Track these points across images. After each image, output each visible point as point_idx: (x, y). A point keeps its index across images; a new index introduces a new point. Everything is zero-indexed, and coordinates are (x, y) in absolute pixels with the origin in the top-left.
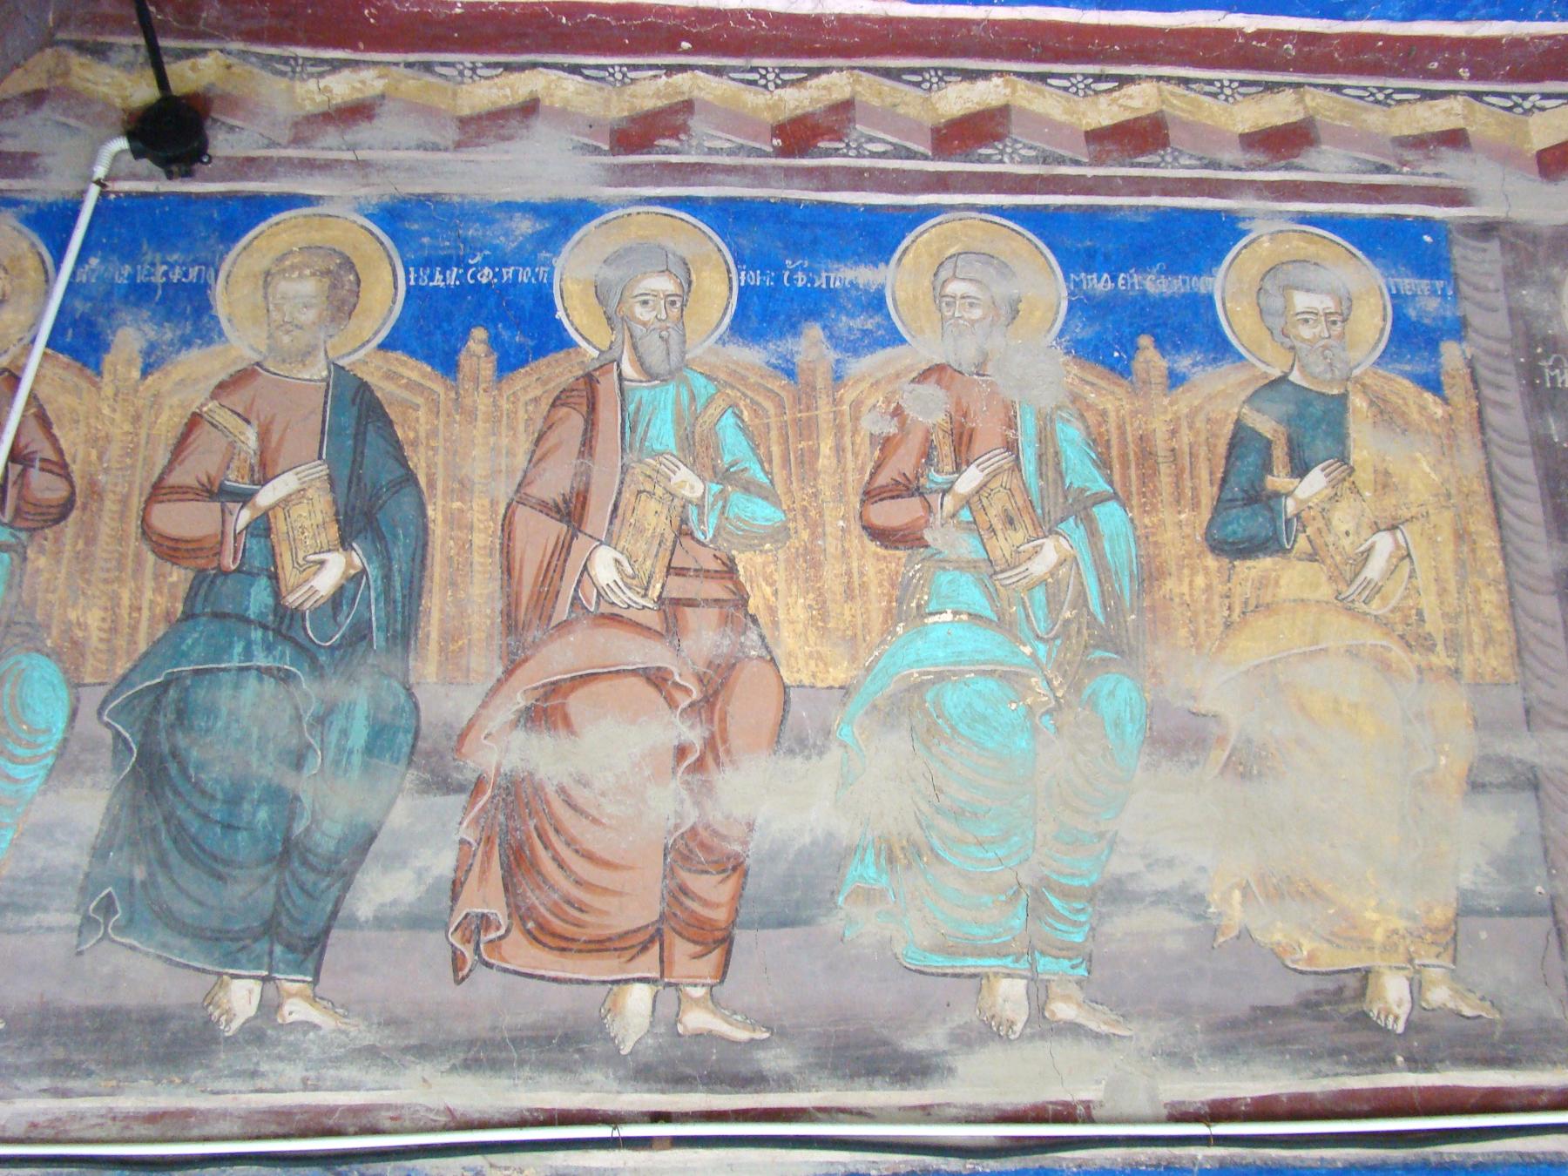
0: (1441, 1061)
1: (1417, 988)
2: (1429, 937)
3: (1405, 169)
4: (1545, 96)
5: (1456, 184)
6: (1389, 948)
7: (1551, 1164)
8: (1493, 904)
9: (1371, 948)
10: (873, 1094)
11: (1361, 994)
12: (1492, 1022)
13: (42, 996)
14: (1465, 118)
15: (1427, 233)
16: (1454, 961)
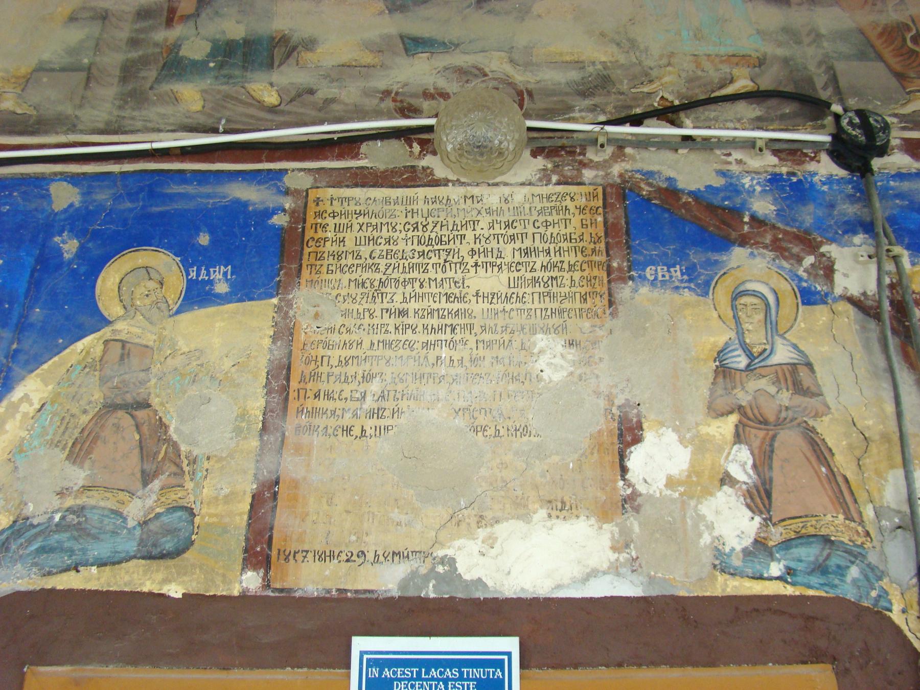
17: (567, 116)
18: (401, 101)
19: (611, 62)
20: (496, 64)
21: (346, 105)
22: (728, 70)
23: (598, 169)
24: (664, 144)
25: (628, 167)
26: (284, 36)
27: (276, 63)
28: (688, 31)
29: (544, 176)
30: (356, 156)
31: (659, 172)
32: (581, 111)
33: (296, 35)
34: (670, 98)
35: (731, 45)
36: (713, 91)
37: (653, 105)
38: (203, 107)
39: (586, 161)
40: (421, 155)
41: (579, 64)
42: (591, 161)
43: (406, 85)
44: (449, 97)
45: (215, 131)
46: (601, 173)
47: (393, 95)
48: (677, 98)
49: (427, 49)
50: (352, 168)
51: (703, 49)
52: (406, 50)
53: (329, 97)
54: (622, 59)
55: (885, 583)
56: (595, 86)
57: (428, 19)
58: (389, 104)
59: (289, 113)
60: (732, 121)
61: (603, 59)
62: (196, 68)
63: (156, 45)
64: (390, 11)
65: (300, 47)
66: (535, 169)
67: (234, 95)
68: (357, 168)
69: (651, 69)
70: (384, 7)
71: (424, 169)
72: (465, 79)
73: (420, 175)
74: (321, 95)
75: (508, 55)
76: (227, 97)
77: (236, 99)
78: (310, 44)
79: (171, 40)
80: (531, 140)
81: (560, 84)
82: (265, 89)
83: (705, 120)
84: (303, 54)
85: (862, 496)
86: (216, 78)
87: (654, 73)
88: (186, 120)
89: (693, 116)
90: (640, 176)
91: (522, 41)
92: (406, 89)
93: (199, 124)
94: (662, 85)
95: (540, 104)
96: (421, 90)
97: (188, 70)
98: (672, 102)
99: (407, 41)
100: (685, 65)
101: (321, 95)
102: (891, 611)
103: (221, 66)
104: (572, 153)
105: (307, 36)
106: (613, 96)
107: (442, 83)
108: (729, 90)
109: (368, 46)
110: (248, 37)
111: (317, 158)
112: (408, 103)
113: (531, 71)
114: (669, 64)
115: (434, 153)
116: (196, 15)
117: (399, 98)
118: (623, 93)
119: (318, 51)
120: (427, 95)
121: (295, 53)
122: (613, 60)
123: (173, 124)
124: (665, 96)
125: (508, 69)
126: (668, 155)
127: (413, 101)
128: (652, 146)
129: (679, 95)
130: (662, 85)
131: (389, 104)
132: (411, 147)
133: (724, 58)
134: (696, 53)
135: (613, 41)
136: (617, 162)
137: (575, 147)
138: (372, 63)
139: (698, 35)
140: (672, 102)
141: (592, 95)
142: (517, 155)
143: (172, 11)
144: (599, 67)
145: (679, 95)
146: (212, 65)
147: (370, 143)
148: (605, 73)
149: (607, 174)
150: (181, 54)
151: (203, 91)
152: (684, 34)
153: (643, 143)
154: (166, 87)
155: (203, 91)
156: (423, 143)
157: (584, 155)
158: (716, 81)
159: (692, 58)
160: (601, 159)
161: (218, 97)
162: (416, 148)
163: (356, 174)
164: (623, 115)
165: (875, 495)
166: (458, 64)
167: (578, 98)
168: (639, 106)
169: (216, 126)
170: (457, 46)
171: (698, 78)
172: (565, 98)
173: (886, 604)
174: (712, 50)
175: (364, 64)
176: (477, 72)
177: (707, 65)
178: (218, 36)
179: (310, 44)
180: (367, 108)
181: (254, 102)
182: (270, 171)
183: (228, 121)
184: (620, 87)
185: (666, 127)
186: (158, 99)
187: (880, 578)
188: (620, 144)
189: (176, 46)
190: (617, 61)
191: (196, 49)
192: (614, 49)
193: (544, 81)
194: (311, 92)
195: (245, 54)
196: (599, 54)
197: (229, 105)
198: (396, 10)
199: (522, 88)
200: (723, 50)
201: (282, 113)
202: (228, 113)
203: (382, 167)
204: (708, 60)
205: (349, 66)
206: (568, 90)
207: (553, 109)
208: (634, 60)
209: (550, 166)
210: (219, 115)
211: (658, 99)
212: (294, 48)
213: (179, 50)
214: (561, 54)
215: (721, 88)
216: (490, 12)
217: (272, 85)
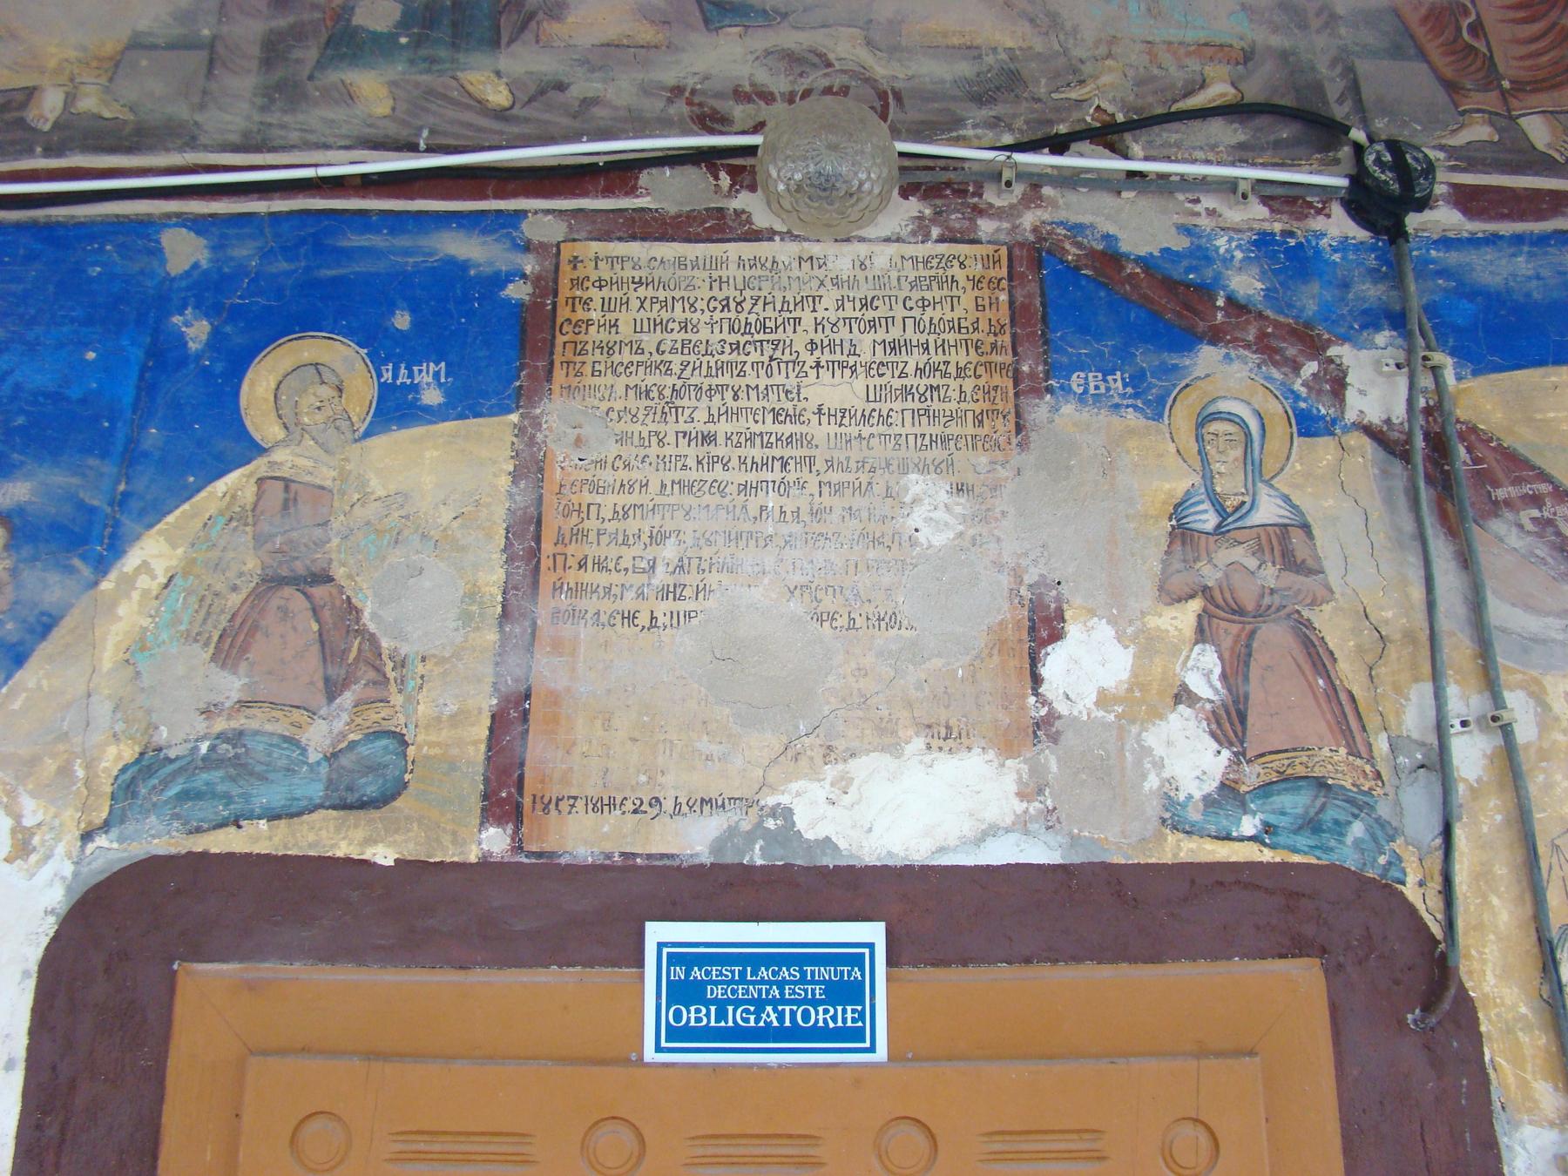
0: (71, 150)
1: (70, 99)
2: (94, 64)
6: (58, 71)
7: (141, 223)
8: (161, 41)
9: (43, 73)
11: (24, 105)
12: (125, 122)
13: (844, 784)
16: (111, 80)
17: (954, 134)
18: (700, 105)
19: (1021, 49)
20: (846, 48)
21: (616, 108)
22: (1197, 68)
23: (1000, 219)
25: (1046, 216)
27: (504, 40)
30: (632, 191)
31: (1092, 226)
32: (975, 126)
34: (1111, 109)
36: (1175, 101)
38: (393, 109)
40: (733, 191)
41: (972, 51)
42: (991, 206)
43: (707, 78)
44: (774, 100)
45: (412, 148)
46: (1006, 225)
48: (1121, 110)
49: (738, 21)
51: (1162, 33)
52: (706, 22)
53: (590, 95)
55: (1398, 845)
56: (999, 86)
58: (680, 108)
59: (527, 120)
61: (1010, 44)
66: (906, 216)
67: (441, 90)
69: (1082, 61)
71: (738, 213)
74: (576, 92)
76: (430, 93)
77: (445, 97)
81: (943, 82)
84: (545, 24)
85: (1372, 722)
86: (412, 62)
87: (1087, 69)
88: (368, 130)
92: (707, 85)
93: (387, 136)
95: (913, 114)
100: (1134, 57)
101: (576, 92)
102: (1403, 883)
103: (418, 43)
104: (962, 193)
106: (1025, 104)
107: (763, 77)
111: (573, 194)
114: (1109, 56)
115: (753, 188)
117: (696, 100)
118: (1039, 100)
119: (570, 19)
120: (739, 95)
121: (533, 24)
122: (1024, 46)
125: (864, 55)
126: (1106, 200)
127: (718, 105)
131: (680, 108)
132: (717, 178)
144: (1003, 56)
145: (1125, 107)
146: (403, 40)
147: (654, 171)
149: (1015, 227)
151: (393, 84)
153: (1070, 180)
154: (333, 76)
156: (734, 172)
157: (980, 196)
160: (1005, 204)
162: (725, 180)
164: (1039, 135)
165: (1392, 720)
168: (1063, 121)
169: (414, 140)
170: (785, 16)
171: (1154, 78)
173: (1398, 875)
174: (1174, 34)
176: (816, 60)
177: (1166, 59)
182: (499, 212)
183: (432, 132)
187: (1392, 839)
188: (1035, 182)
192: (1027, 27)
194: (561, 87)
195: (454, 24)
197: (434, 107)
200: (1191, 36)
201: (515, 120)
202: (431, 120)
208: (1057, 47)
209: (927, 212)
212: (531, 16)
214: (945, 35)
215: (1185, 96)
217: (498, 74)
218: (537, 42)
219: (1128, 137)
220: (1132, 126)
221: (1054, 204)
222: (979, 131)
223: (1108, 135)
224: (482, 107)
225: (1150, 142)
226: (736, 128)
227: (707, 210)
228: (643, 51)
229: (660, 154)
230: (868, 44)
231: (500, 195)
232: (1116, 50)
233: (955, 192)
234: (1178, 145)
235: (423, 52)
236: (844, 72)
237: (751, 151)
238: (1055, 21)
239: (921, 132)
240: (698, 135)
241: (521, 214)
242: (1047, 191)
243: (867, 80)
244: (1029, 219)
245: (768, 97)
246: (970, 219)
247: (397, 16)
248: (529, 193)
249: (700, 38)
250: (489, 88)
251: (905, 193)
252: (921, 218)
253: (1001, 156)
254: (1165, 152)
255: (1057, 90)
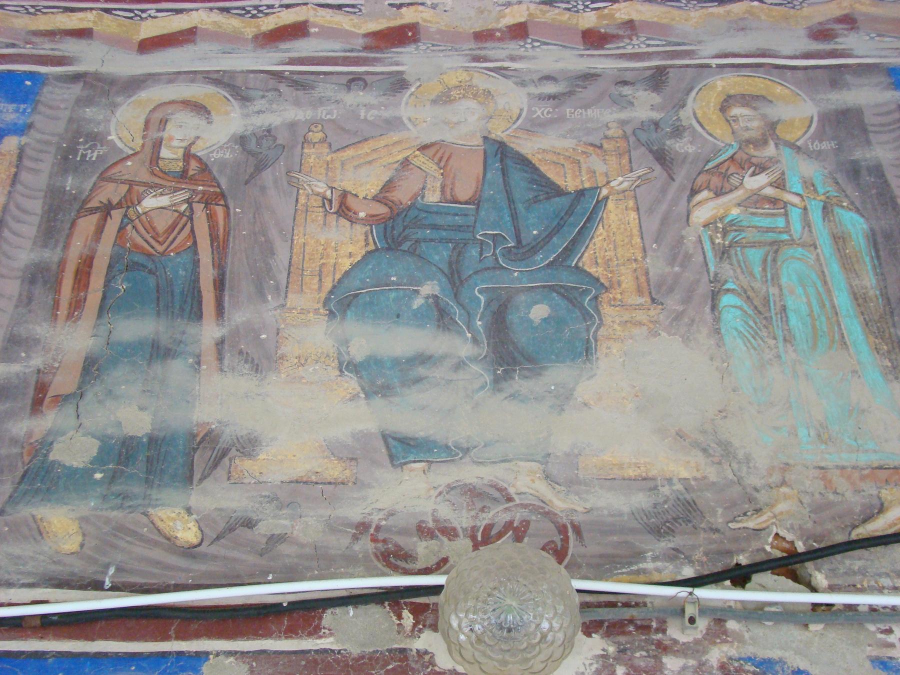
3: (28, 46)
4: (158, 11)
5: (66, 54)
10: (279, 642)
14: (94, 22)
15: (29, 80)
17: (635, 568)
18: (385, 541)
19: (695, 479)
20: (526, 482)
21: (303, 546)
22: (874, 492)
23: (685, 656)
24: (788, 615)
25: (733, 652)
26: (209, 433)
27: (197, 476)
28: (808, 428)
29: (604, 667)
30: (316, 632)
31: (781, 661)
32: (655, 559)
33: (228, 431)
34: (789, 537)
35: (875, 451)
36: (855, 527)
37: (764, 550)
38: (82, 546)
39: (667, 643)
40: (416, 631)
41: (648, 483)
42: (675, 642)
43: (391, 514)
44: (456, 535)
45: (97, 586)
46: (692, 662)
47: (372, 531)
48: (800, 538)
49: (422, 456)
50: (309, 651)
51: (832, 458)
52: (392, 457)
53: (277, 532)
54: (712, 474)
56: (677, 515)
57: (423, 408)
58: (365, 545)
59: (215, 558)
60: (887, 575)
61: (685, 474)
62: (74, 481)
63: (14, 441)
64: (367, 396)
65: (234, 449)
66: (590, 654)
67: (132, 527)
68: (317, 651)
69: (757, 490)
70: (359, 389)
71: (421, 654)
72: (479, 505)
73: (413, 665)
74: (263, 529)
75: (542, 467)
76: (120, 529)
77: (134, 534)
78: (248, 446)
79: (37, 436)
80: (585, 606)
81: (621, 514)
82: (178, 518)
83: (846, 573)
84: (237, 461)
86: (104, 498)
87: (762, 497)
88: (53, 567)
89: (826, 567)
90: (752, 668)
91: (562, 444)
92: (391, 521)
93: (73, 574)
94: (775, 516)
95: (593, 548)
96: (414, 522)
97: (61, 483)
98: (792, 543)
99: (390, 440)
100: (808, 483)
101: (263, 529)
103: (112, 478)
104: (645, 628)
105: (244, 432)
106: (703, 535)
107: (445, 512)
108: (878, 526)
109: (334, 450)
110: (156, 433)
111: (256, 634)
112: (396, 545)
113: (577, 494)
114: (784, 483)
115: (434, 628)
116: (80, 394)
117: (381, 536)
118: (717, 531)
119: (261, 457)
120: (424, 532)
121: (226, 460)
122: (699, 475)
123: (29, 574)
124: (781, 534)
125: (543, 489)
126: (792, 633)
127: (401, 541)
128: (768, 620)
129: (807, 536)
130: (775, 516)
131: (365, 545)
132: (400, 617)
133: (866, 472)
134: (823, 464)
135: (696, 445)
136: (715, 643)
137: (651, 620)
138: (342, 477)
139: (823, 436)
140: (792, 543)
141: (671, 532)
142: (568, 645)
143: (42, 389)
144: (679, 487)
145: (807, 536)
146: (98, 476)
147: (338, 610)
148: (688, 497)
149: (702, 664)
150: (51, 457)
151: (84, 520)
152: (802, 432)
153: (755, 613)
154: (25, 511)
155: (84, 520)
156: (418, 611)
157: (664, 631)
158: (858, 509)
159: (817, 473)
160: (690, 639)
161: (106, 529)
162: (408, 619)
163: (315, 661)
164: (718, 567)
166: (468, 482)
167: (650, 537)
168: (743, 551)
169: (99, 577)
170: (466, 451)
171: (830, 505)
172: (630, 538)
174: (846, 458)
175: (329, 479)
176: (497, 494)
177: (842, 485)
178: (110, 431)
179: (248, 446)
180: (333, 552)
181: (157, 538)
182: (180, 654)
183: (119, 570)
184: (712, 520)
185: (800, 591)
186: (10, 531)
188: (719, 616)
189: (46, 444)
190: (705, 478)
191: (75, 451)
192: (700, 457)
193: (598, 509)
194: (249, 524)
195: (149, 460)
196: (680, 467)
197: (123, 544)
198: (376, 393)
199: (565, 520)
200: (863, 459)
201: (204, 557)
202: (119, 557)
203: (355, 651)
204: (842, 476)
205: (306, 483)
206: (634, 524)
207: (614, 556)
208: (731, 476)
209: (611, 649)
210: (107, 560)
211: (770, 539)
212: (225, 453)
213: (48, 451)
214: (621, 466)
215: (865, 521)
216: (512, 396)
217: (189, 511)
218: (229, 479)
219: (810, 565)
220: (814, 555)
221: (739, 638)
222: (659, 564)
223: (790, 565)
224: (170, 543)
225: (833, 570)
226: (420, 565)
227: (390, 651)
228: (331, 487)
229: (345, 594)
230: (547, 477)
231: (182, 636)
232: (790, 477)
233: (638, 628)
234: (863, 572)
235: (116, 488)
236: (525, 506)
237: (436, 590)
238: (727, 451)
239: (603, 567)
240: (383, 575)
241: (202, 656)
242: (732, 625)
243: (547, 514)
244: (715, 655)
245: (450, 532)
246: (655, 657)
247: (94, 452)
248: (211, 634)
249: (386, 474)
250: (179, 525)
251: (589, 629)
252: (605, 657)
253: (682, 592)
254: (850, 580)
255: (734, 520)
